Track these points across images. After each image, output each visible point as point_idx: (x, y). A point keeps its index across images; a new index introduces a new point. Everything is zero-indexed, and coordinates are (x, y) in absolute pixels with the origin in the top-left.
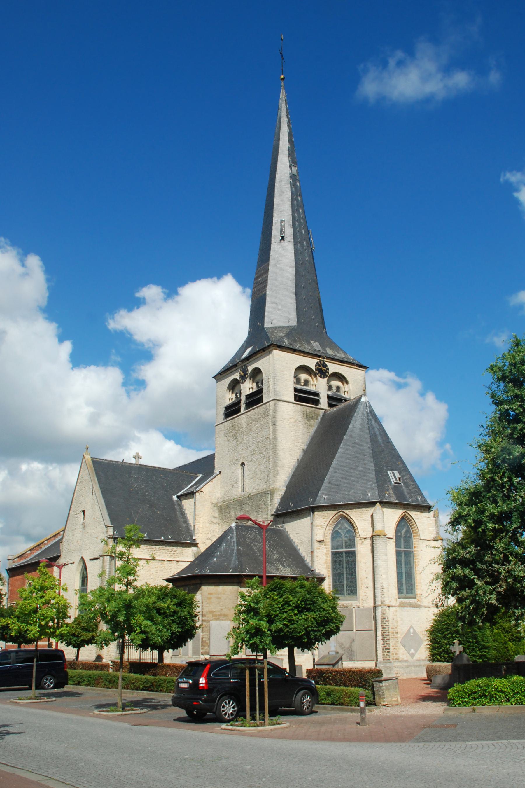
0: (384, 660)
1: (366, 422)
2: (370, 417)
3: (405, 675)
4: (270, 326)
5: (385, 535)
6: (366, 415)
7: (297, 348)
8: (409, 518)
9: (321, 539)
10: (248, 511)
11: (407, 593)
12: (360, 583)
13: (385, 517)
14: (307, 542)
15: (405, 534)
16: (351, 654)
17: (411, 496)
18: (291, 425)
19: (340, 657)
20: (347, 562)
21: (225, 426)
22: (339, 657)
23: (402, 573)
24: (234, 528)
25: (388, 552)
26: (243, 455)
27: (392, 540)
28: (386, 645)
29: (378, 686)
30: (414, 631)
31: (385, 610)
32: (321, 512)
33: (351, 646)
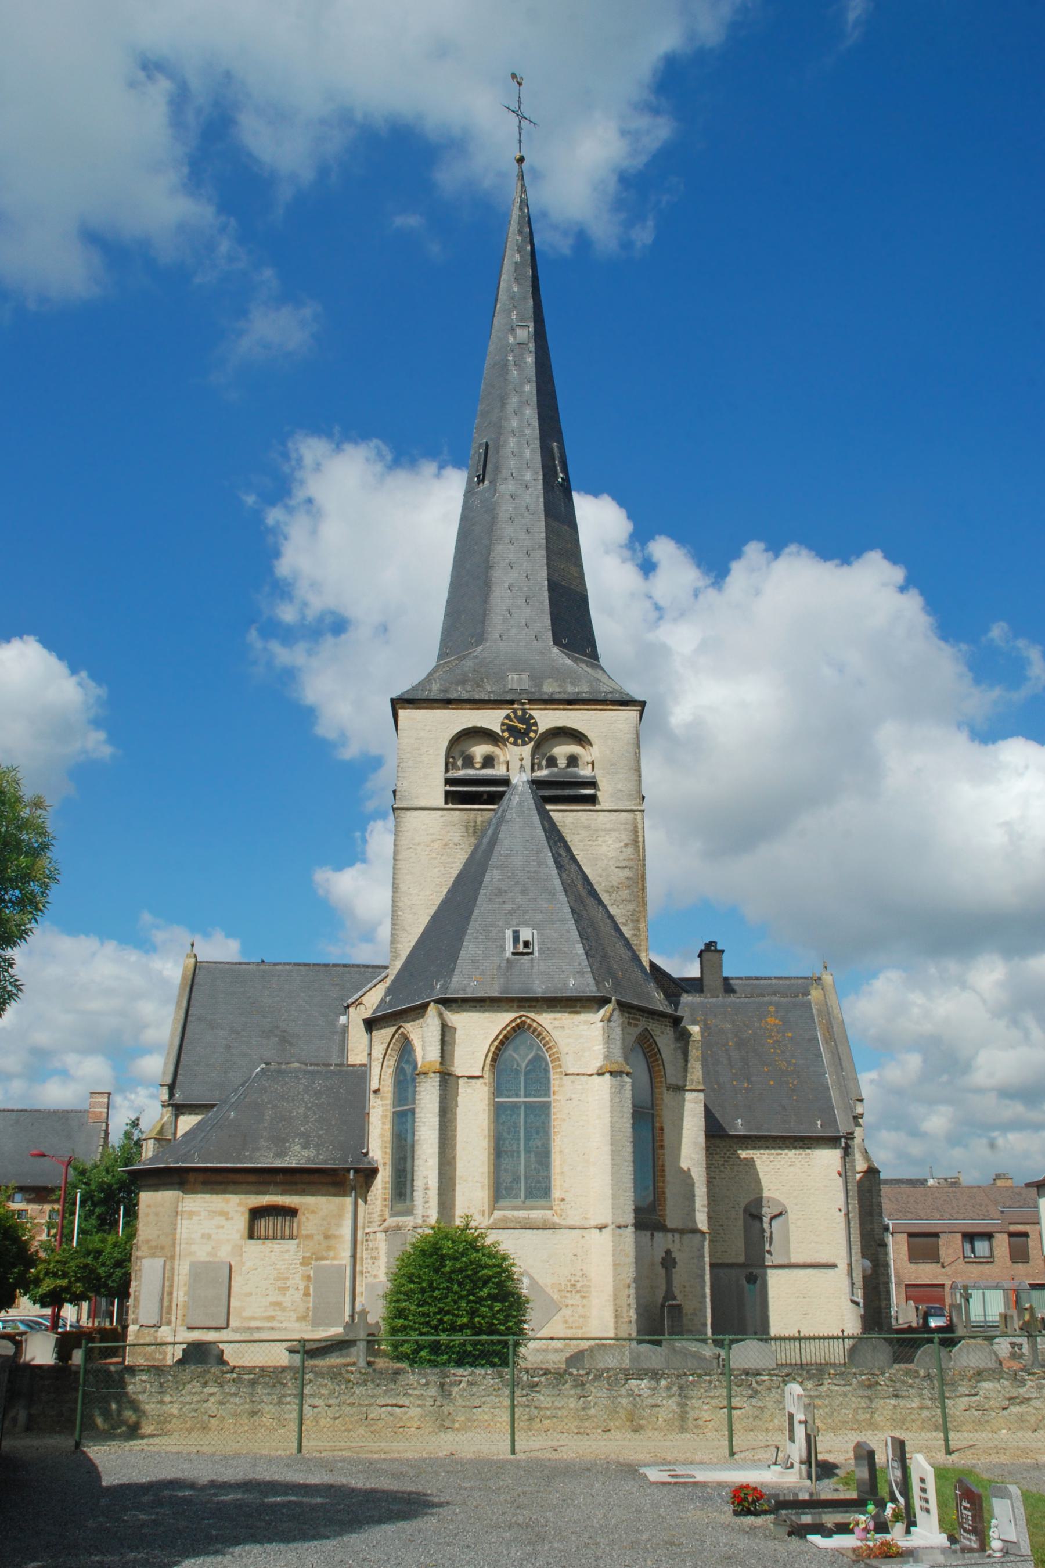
8: (530, 1026)
18: (434, 855)
27: (481, 1080)
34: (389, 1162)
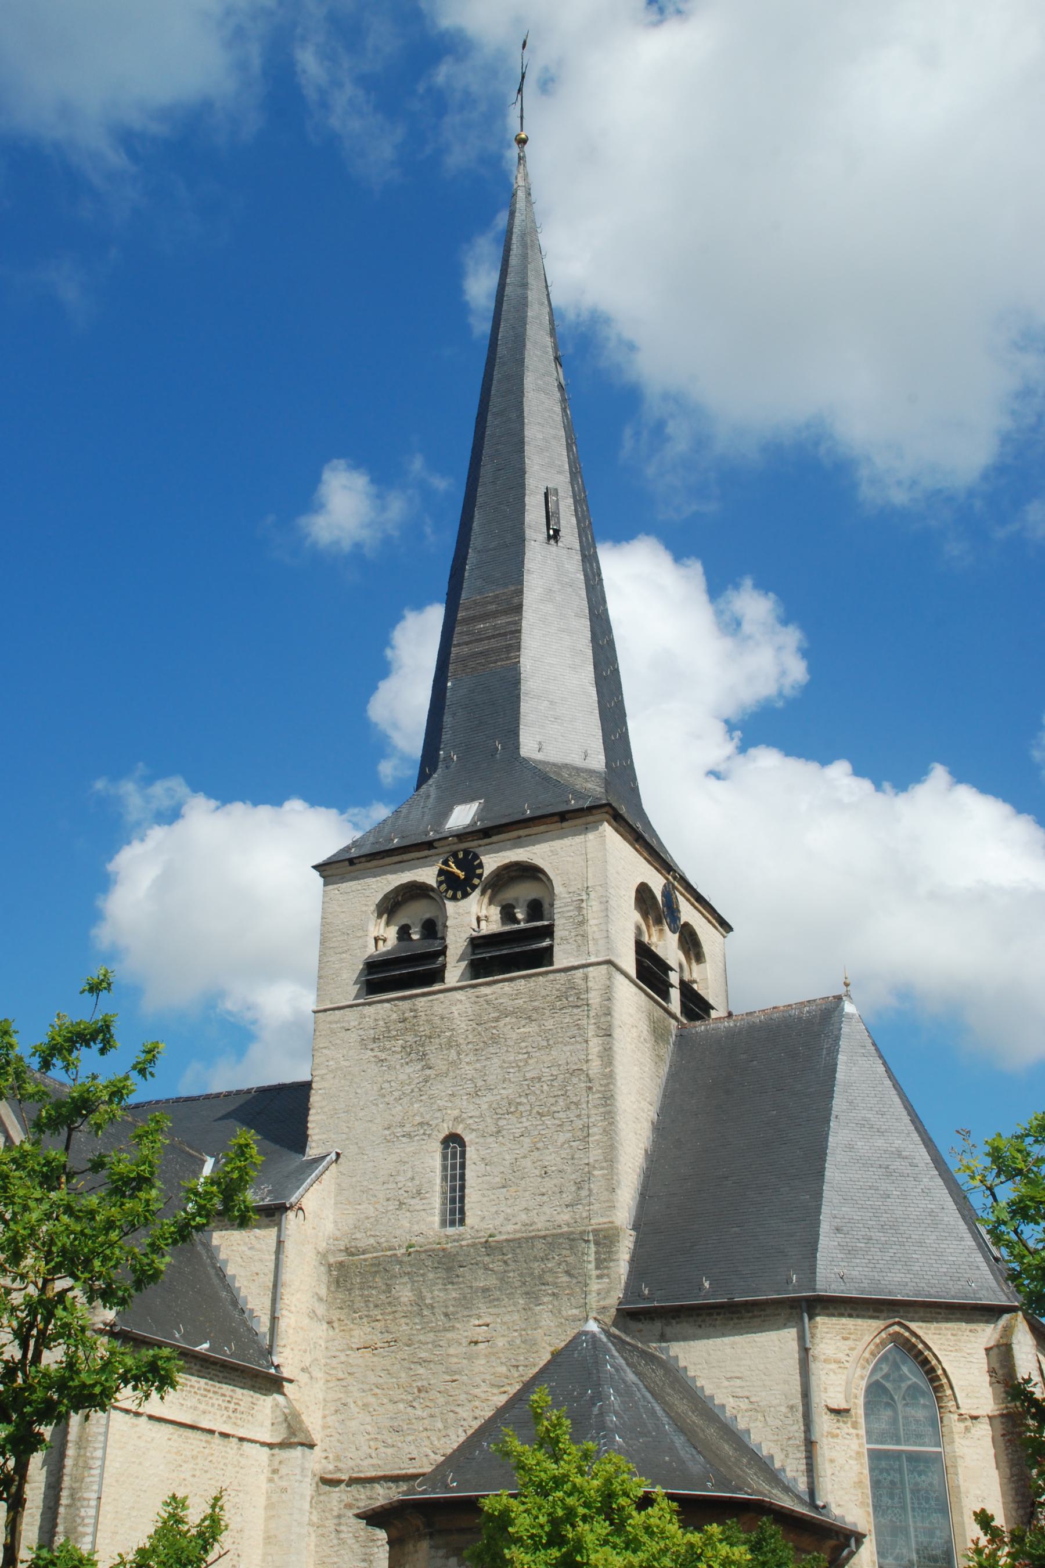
9: (839, 1403)
32: (834, 1320)
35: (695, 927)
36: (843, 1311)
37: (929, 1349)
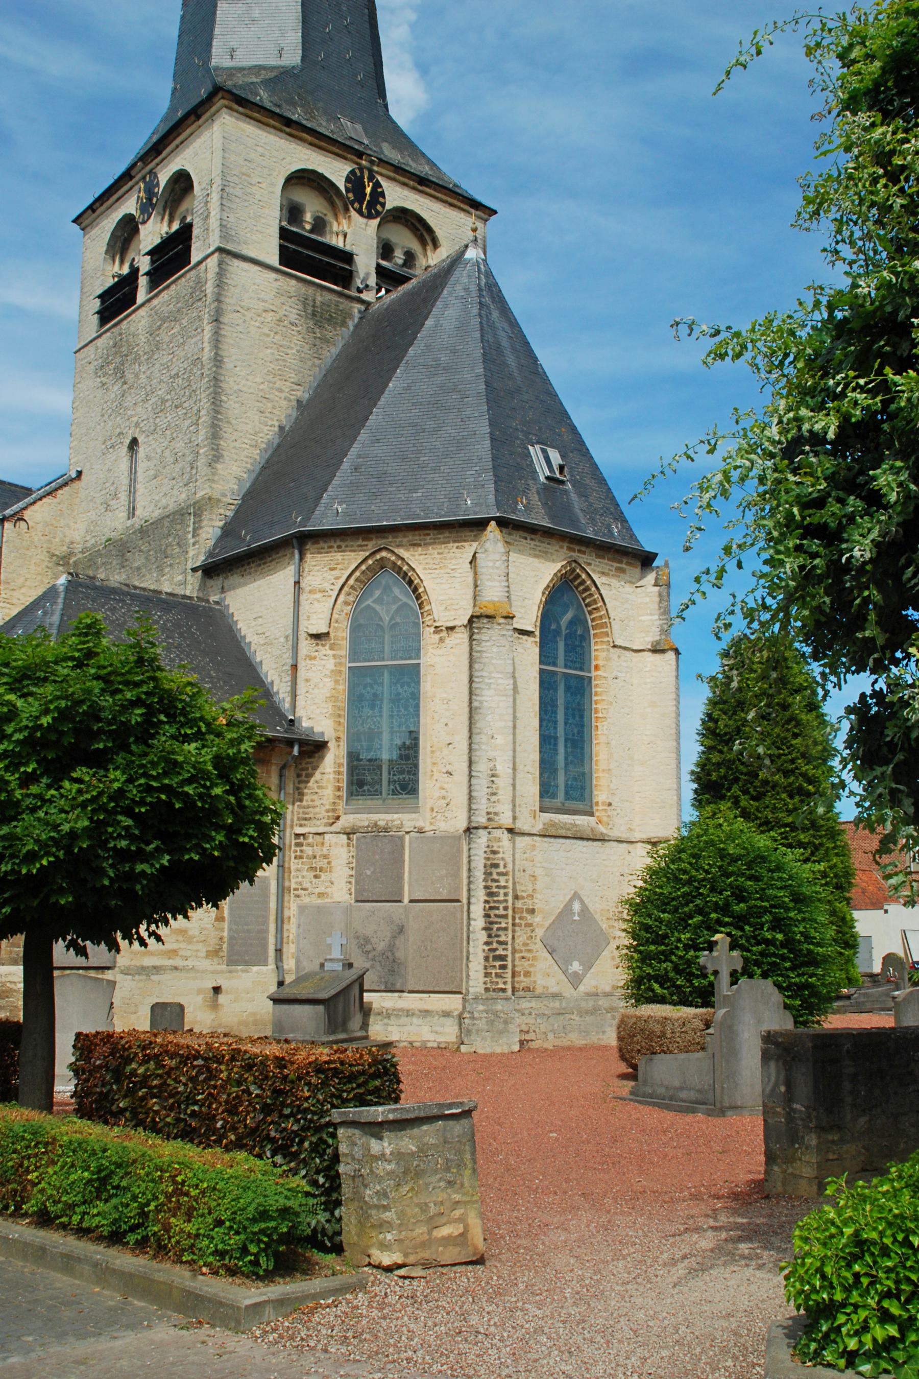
0: (487, 990)
1: (475, 311)
2: (487, 300)
3: (551, 1036)
4: (227, 63)
5: (510, 617)
6: (475, 293)
7: (295, 117)
8: (583, 582)
10: (138, 569)
11: (568, 796)
12: (429, 760)
13: (511, 569)
14: (282, 640)
15: (567, 630)
16: (392, 971)
17: (593, 520)
18: (266, 330)
19: (355, 977)
20: (396, 700)
21: (97, 348)
22: (352, 974)
23: (556, 738)
24: (61, 588)
25: (516, 667)
26: (135, 419)
27: (531, 639)
28: (495, 945)
29: (358, 1152)
30: (585, 910)
31: (499, 840)
33: (391, 947)
34: (344, 737)
35: (418, 211)
36: (332, 543)
37: (414, 570)
